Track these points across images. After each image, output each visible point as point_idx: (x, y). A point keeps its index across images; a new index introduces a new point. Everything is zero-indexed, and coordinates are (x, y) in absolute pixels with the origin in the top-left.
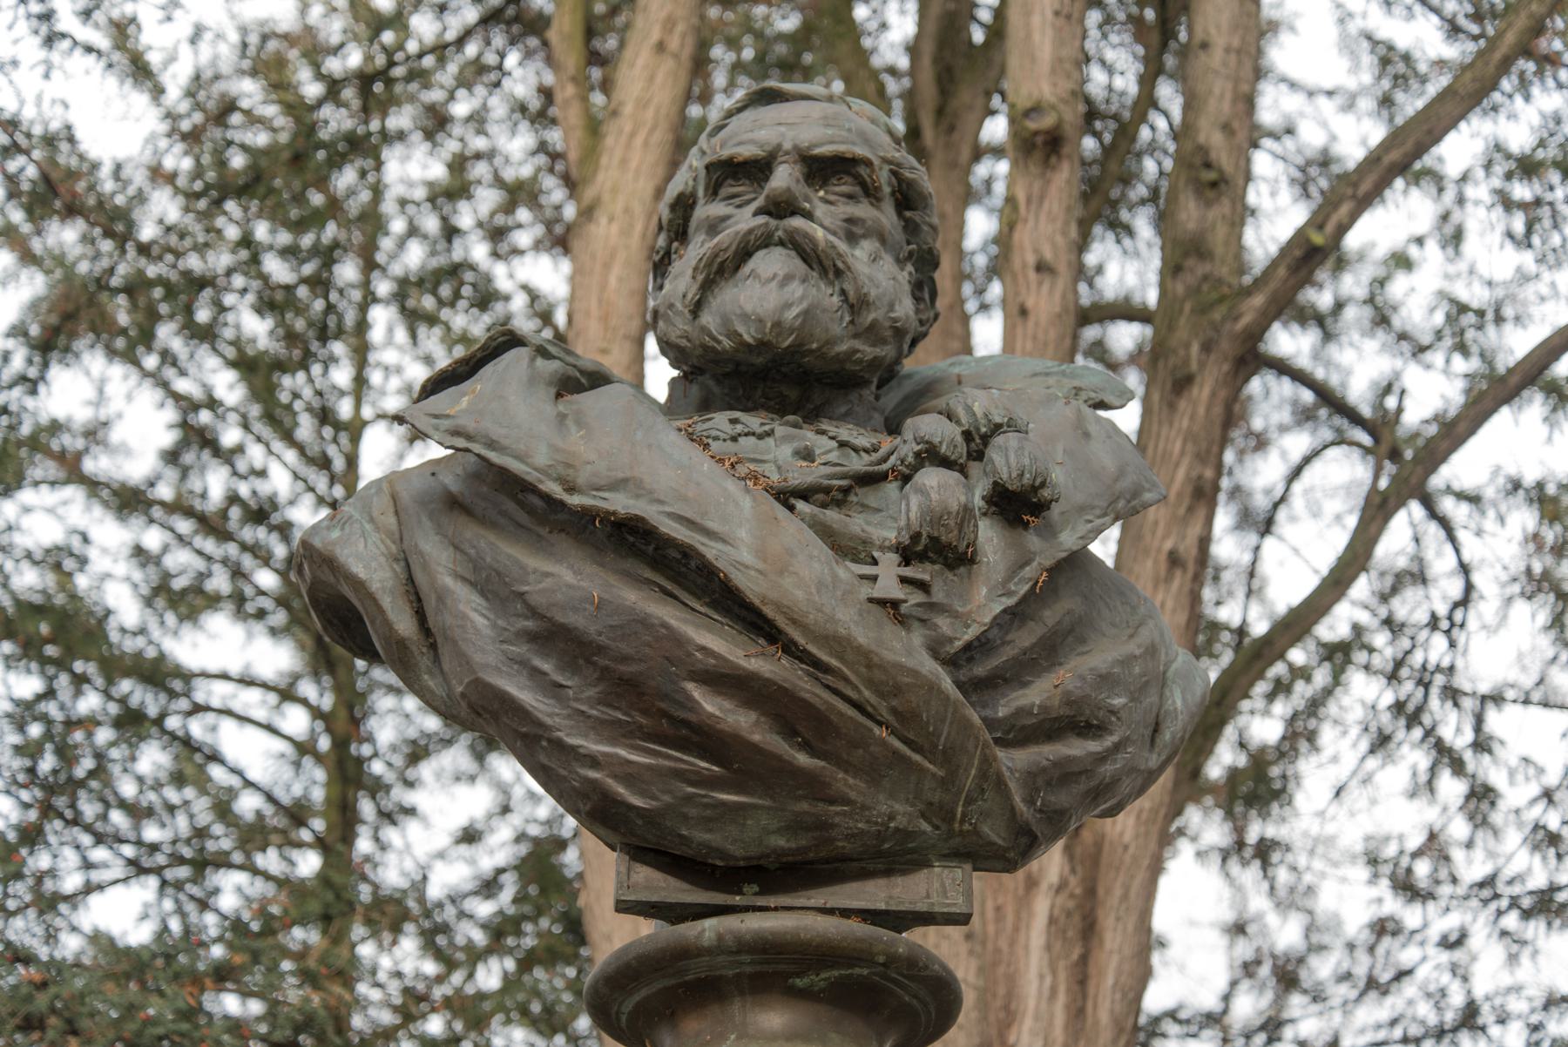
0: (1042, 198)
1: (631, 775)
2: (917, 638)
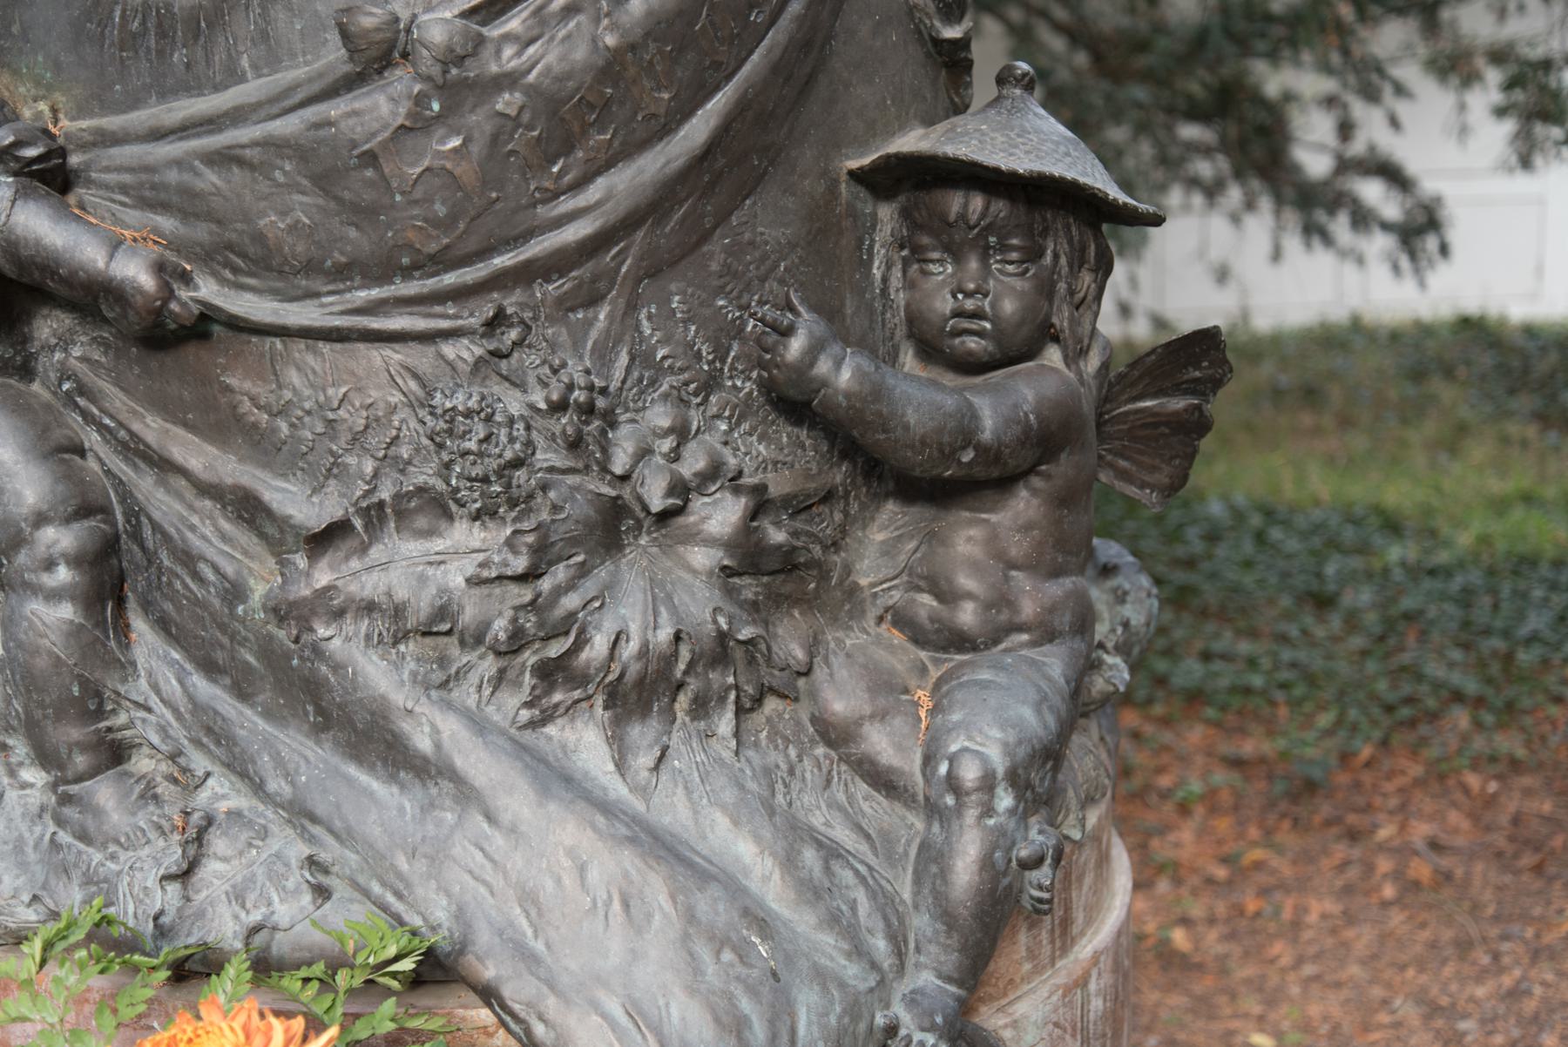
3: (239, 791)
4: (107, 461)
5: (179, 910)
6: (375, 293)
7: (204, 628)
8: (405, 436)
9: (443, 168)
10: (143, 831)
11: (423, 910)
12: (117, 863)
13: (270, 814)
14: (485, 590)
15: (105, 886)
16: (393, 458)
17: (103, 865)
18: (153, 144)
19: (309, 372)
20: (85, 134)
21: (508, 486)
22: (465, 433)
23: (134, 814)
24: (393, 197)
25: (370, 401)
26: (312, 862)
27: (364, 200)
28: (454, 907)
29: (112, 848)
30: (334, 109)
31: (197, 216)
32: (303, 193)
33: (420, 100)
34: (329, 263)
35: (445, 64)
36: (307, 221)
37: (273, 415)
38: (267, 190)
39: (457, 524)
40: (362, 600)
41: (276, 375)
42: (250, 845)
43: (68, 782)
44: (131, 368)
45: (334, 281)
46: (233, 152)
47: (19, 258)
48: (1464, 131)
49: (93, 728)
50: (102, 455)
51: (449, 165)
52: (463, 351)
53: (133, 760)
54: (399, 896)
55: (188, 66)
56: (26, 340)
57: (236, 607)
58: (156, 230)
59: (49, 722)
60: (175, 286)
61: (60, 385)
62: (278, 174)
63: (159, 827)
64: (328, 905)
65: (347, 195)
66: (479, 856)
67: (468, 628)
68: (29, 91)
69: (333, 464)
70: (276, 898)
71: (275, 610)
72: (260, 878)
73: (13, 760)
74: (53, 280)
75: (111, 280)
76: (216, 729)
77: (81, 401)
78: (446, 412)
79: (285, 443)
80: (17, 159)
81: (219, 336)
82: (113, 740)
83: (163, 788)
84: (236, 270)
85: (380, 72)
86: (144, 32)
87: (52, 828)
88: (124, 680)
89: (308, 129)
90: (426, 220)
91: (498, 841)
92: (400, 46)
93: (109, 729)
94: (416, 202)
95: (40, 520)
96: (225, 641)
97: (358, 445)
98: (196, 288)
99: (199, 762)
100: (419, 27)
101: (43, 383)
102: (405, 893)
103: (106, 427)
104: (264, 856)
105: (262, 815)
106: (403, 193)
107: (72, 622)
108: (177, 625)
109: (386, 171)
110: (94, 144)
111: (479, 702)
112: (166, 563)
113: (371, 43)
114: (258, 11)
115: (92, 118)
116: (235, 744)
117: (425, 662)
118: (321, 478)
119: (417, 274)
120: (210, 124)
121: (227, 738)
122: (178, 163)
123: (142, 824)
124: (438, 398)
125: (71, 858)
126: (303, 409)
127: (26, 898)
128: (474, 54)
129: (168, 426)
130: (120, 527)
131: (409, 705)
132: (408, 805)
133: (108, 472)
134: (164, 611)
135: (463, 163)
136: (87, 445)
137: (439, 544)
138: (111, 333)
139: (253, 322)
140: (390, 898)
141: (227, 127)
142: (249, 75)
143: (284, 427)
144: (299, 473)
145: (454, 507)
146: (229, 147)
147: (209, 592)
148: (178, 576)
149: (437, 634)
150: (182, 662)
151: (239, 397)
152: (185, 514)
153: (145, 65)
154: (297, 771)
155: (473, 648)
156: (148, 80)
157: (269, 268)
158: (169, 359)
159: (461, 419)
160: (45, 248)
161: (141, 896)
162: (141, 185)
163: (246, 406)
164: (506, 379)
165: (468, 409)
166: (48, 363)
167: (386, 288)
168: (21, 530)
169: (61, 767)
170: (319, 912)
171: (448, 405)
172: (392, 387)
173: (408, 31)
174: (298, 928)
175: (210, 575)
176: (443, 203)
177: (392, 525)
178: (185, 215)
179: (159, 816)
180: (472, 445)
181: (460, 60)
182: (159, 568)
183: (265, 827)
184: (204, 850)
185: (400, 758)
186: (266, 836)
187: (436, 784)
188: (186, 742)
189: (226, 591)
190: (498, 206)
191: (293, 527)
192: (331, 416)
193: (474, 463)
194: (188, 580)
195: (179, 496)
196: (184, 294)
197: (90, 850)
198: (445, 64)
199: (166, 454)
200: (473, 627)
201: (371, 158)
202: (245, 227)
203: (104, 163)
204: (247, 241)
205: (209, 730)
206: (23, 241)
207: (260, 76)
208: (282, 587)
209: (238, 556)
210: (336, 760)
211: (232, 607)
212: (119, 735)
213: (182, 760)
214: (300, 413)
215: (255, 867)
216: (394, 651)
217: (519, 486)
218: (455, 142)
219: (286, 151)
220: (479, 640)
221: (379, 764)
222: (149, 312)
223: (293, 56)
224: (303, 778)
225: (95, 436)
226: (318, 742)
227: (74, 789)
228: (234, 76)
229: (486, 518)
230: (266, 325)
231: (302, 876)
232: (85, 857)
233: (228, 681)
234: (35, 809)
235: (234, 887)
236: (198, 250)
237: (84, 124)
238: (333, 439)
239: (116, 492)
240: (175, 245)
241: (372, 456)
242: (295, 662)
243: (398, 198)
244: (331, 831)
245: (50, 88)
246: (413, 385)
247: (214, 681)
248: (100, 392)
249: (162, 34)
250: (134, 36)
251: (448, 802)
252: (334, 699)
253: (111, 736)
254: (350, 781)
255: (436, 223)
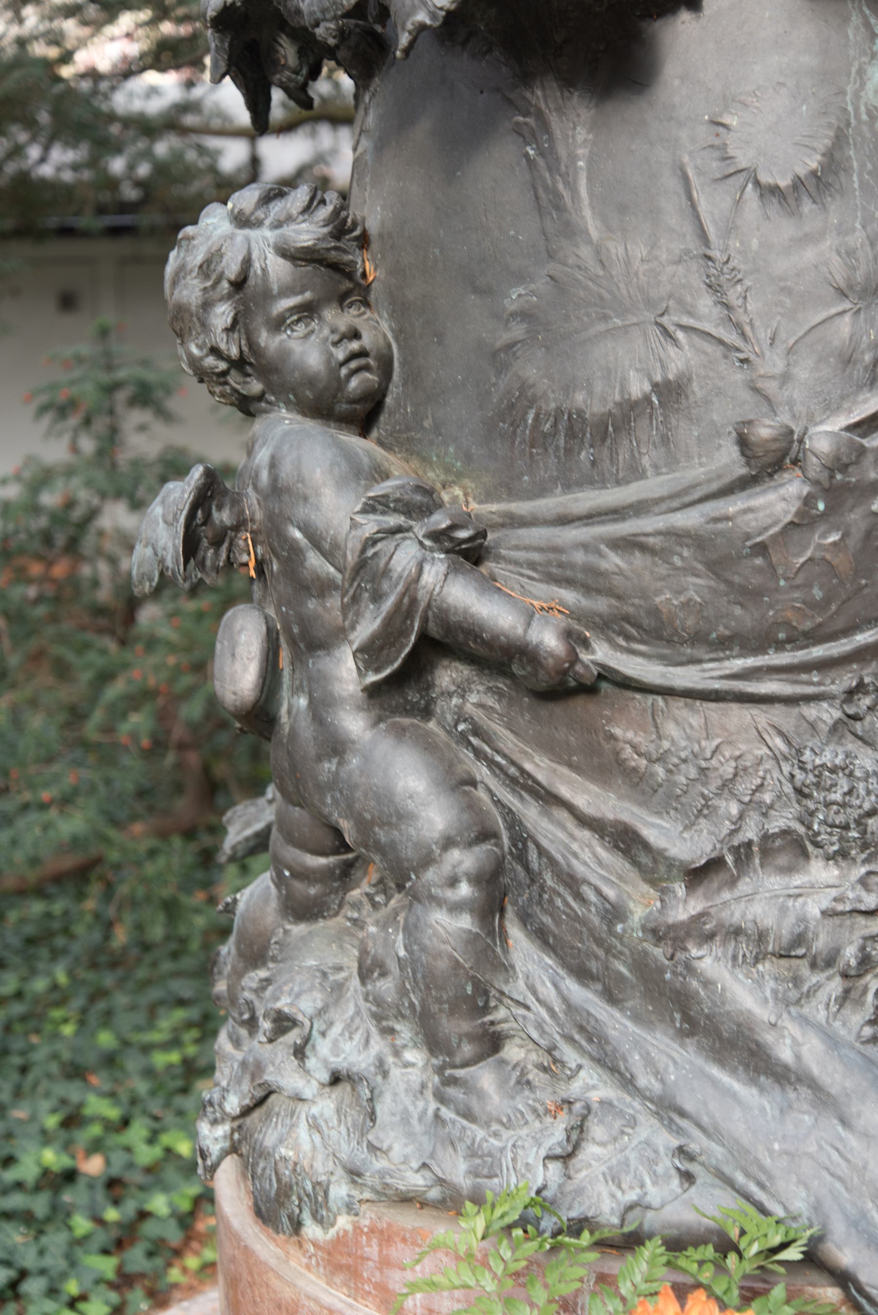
3: (605, 1083)
4: (497, 793)
5: (560, 1186)
6: (751, 662)
7: (581, 941)
8: (769, 784)
9: (823, 559)
10: (522, 1113)
11: (784, 1200)
12: (500, 1140)
13: (636, 1104)
14: (837, 920)
15: (489, 1159)
16: (757, 803)
17: (486, 1141)
18: (559, 528)
19: (686, 726)
20: (494, 517)
21: (864, 832)
22: (832, 786)
23: (513, 1098)
24: (778, 582)
25: (737, 753)
26: (681, 1151)
27: (751, 584)
28: (812, 1199)
29: (495, 1127)
30: (733, 505)
31: (599, 591)
32: (697, 576)
33: (808, 501)
34: (714, 635)
35: (831, 471)
36: (699, 600)
37: (651, 761)
38: (664, 572)
39: (813, 862)
40: (731, 925)
41: (656, 727)
42: (623, 1133)
43: (455, 1067)
44: (523, 715)
45: (716, 650)
46: (637, 539)
47: (448, 623)
49: (480, 1021)
50: (492, 787)
51: (828, 557)
53: (506, 1048)
54: (761, 1185)
55: (594, 463)
56: (430, 686)
57: (615, 925)
58: (562, 603)
59: (444, 1016)
60: (578, 650)
61: (456, 726)
62: (677, 561)
63: (535, 1111)
64: (693, 1190)
65: (737, 579)
66: (835, 1156)
67: (821, 954)
68: (438, 476)
69: (703, 806)
70: (648, 1181)
71: (654, 931)
72: (633, 1162)
73: (399, 1042)
74: (475, 642)
75: (527, 645)
76: (589, 1028)
77: (474, 741)
78: (815, 768)
79: (660, 785)
80: (452, 539)
81: (606, 691)
82: (494, 1033)
83: (534, 1075)
84: (628, 638)
85: (771, 475)
86: (554, 433)
87: (433, 1105)
88: (507, 982)
89: (708, 523)
90: (804, 602)
91: (853, 1141)
92: (793, 454)
93: (492, 1023)
94: (798, 587)
95: (448, 843)
96: (601, 953)
97: (726, 791)
98: (593, 652)
99: (570, 1056)
100: (810, 438)
101: (439, 723)
102: (768, 1184)
103: (498, 765)
104: (635, 1142)
105: (630, 1106)
106: (786, 579)
107: (470, 931)
108: (555, 936)
109: (774, 559)
110: (503, 525)
111: (828, 1018)
112: (550, 883)
113: (767, 452)
114: (660, 418)
115: (498, 502)
116: (607, 1042)
117: (783, 981)
118: (693, 818)
119: (788, 647)
120: (616, 513)
121: (600, 1038)
122: (585, 546)
123: (520, 1107)
124: (807, 756)
125: (456, 1133)
126: (680, 758)
127: (415, 1165)
128: (857, 462)
129: (554, 765)
130: (506, 849)
131: (773, 1020)
132: (768, 1107)
133: (498, 803)
134: (543, 924)
135: (841, 555)
136: (478, 778)
137: (798, 880)
138: (506, 685)
139: (645, 684)
140: (753, 1188)
141: (630, 517)
142: (649, 474)
143: (660, 771)
144: (672, 812)
145: (810, 848)
146: (634, 535)
147: (590, 911)
148: (559, 895)
149: (796, 957)
150: (555, 967)
151: (621, 744)
152: (567, 841)
153: (552, 460)
154: (666, 1069)
155: (822, 970)
156: (555, 473)
157: (660, 638)
158: (557, 709)
159: (827, 773)
160: (472, 616)
161: (523, 1171)
162: (549, 563)
163: (628, 752)
164: (860, 738)
165: (836, 766)
166: (445, 707)
167: (760, 657)
168: (431, 852)
169: (450, 1053)
170: (686, 1196)
171: (818, 762)
172: (759, 742)
173: (801, 441)
174: (668, 1208)
175: (592, 896)
176: (820, 589)
177: (757, 861)
178: (587, 589)
179: (534, 1100)
180: (837, 796)
181: (844, 468)
182: (542, 888)
183: (634, 1117)
184: (584, 1135)
185: (762, 1064)
186: (635, 1124)
187: (795, 1089)
188: (558, 1037)
189: (607, 911)
190: (866, 591)
191: (666, 858)
192: (703, 764)
193: (837, 813)
194: (570, 899)
195: (564, 828)
196: (585, 657)
197: (474, 1127)
198: (831, 471)
199: (554, 790)
200: (824, 953)
201: (762, 549)
202: (642, 603)
203: (513, 543)
204: (643, 614)
205: (582, 1029)
206: (453, 610)
207: (658, 474)
208: (661, 911)
209: (614, 879)
210: (700, 1061)
211: (611, 924)
212: (498, 1028)
213: (556, 1053)
214: (676, 760)
215: (627, 1152)
216: (754, 970)
217: (873, 833)
218: (834, 537)
219: (686, 540)
220: (830, 962)
221: (741, 1068)
222: (557, 673)
223: (689, 457)
224: (672, 1077)
225: (485, 771)
226: (683, 1045)
227: (460, 1073)
228: (636, 473)
229: (840, 859)
230: (655, 686)
231: (673, 1163)
232: (469, 1133)
233: (599, 987)
234: (417, 1086)
235: (610, 1169)
236: (597, 619)
237: (494, 507)
238: (705, 784)
239: (505, 820)
240: (575, 614)
241: (740, 801)
242: (668, 976)
243: (782, 583)
244: (699, 1126)
245: (459, 475)
246: (778, 743)
247: (586, 986)
248: (495, 734)
249: (571, 434)
250: (545, 436)
251: (806, 1107)
252: (702, 1010)
253: (492, 1029)
254: (715, 1083)
255: (814, 605)
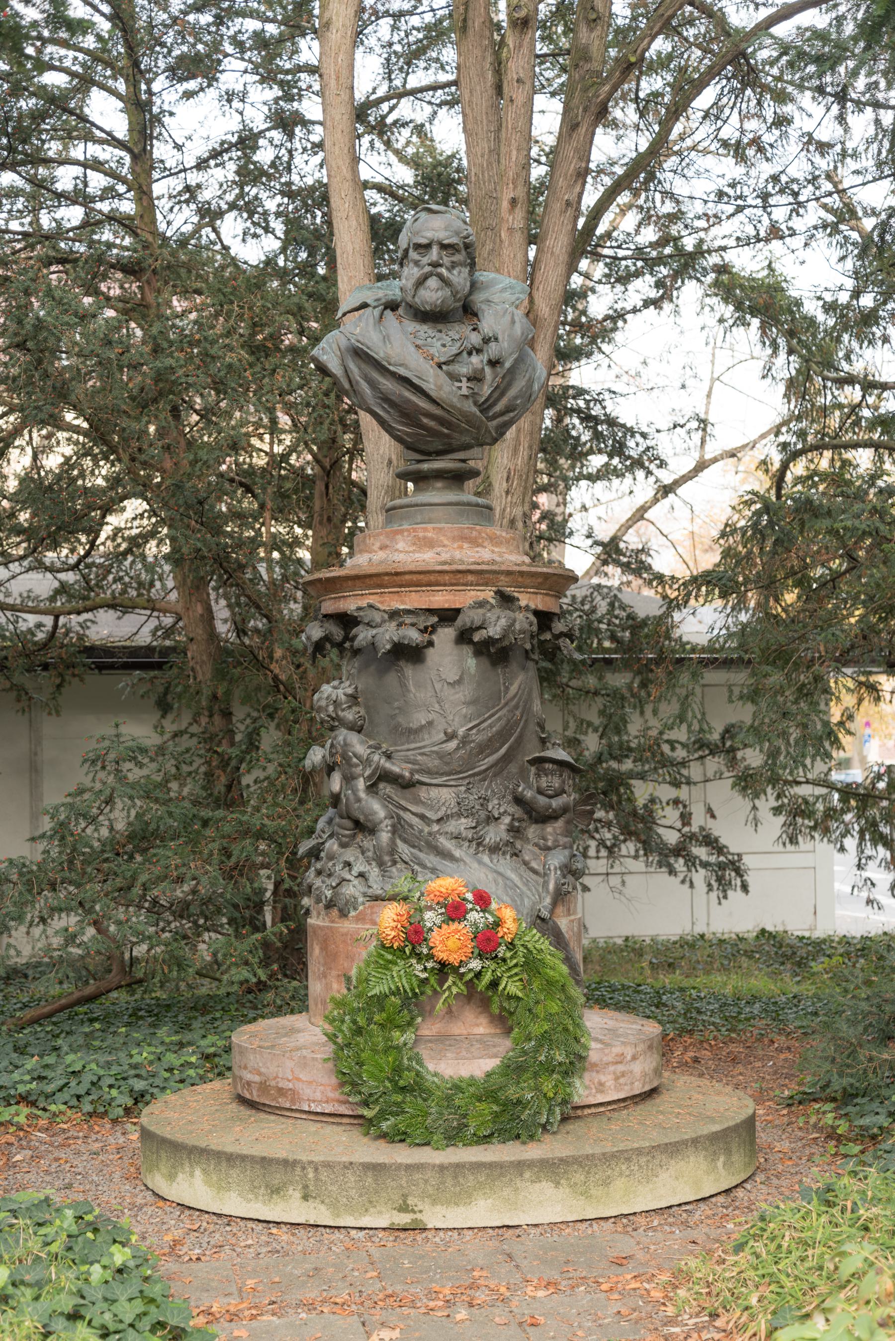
0: (520, 46)
1: (407, 434)
2: (471, 401)
48: (756, 822)
52: (463, 788)
